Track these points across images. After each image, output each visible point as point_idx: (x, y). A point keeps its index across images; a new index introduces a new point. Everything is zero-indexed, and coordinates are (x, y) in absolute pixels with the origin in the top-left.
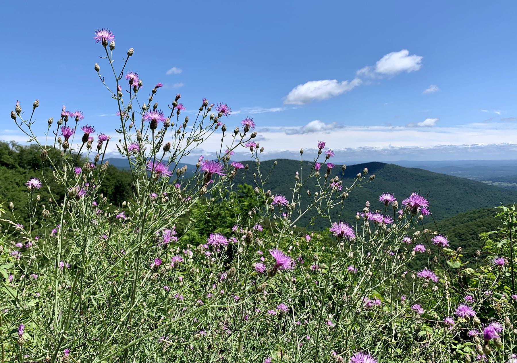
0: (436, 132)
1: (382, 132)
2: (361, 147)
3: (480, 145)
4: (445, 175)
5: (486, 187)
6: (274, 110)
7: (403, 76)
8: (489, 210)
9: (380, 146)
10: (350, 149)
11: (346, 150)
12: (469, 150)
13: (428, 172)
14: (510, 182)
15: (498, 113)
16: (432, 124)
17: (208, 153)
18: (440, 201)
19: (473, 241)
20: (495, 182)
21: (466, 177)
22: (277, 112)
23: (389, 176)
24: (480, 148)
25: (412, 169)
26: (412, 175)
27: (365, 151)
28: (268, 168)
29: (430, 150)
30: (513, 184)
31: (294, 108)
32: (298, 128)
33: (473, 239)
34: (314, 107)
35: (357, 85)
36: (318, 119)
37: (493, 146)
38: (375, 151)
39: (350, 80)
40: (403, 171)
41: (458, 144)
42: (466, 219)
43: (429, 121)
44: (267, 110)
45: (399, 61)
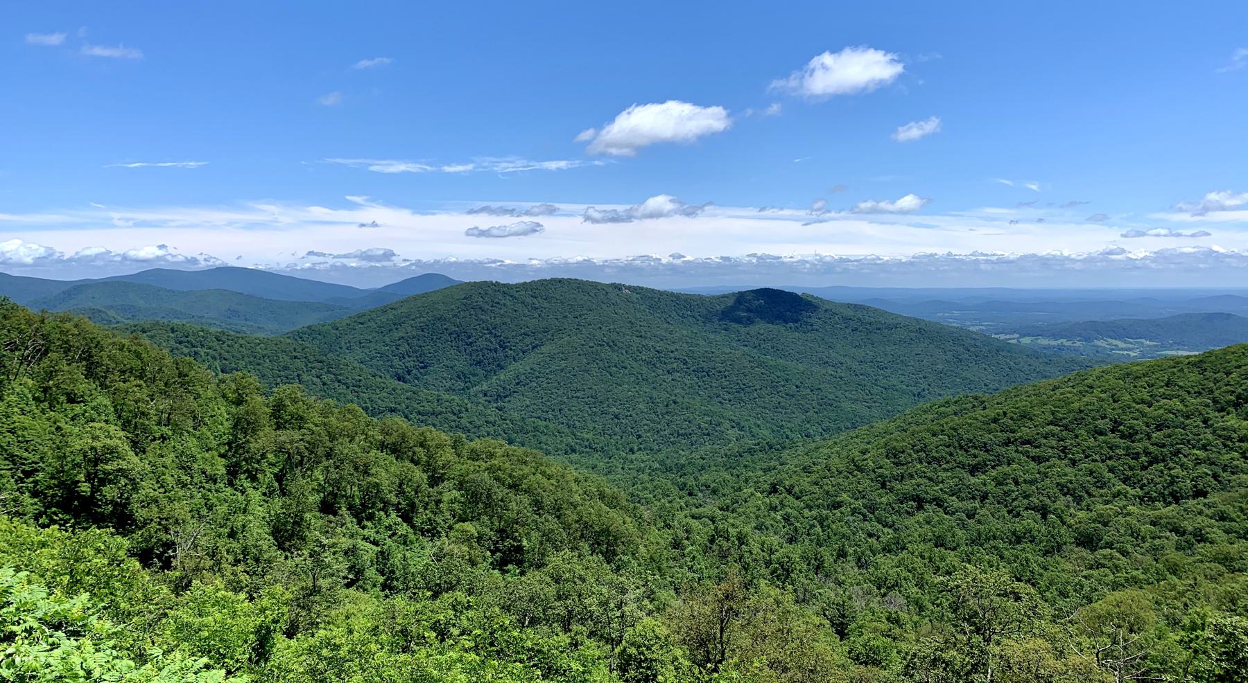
0: (909, 225)
2: (754, 255)
4: (917, 321)
5: (1004, 348)
6: (553, 165)
8: (976, 398)
10: (727, 259)
12: (983, 266)
13: (884, 313)
14: (1055, 336)
15: (1034, 187)
19: (919, 466)
20: (1025, 336)
22: (559, 169)
25: (849, 306)
26: (847, 319)
27: (766, 263)
28: (529, 300)
30: (1059, 342)
32: (621, 208)
33: (921, 462)
34: (660, 163)
36: (667, 193)
41: (961, 251)
43: (908, 201)
44: (537, 166)
45: (857, 69)
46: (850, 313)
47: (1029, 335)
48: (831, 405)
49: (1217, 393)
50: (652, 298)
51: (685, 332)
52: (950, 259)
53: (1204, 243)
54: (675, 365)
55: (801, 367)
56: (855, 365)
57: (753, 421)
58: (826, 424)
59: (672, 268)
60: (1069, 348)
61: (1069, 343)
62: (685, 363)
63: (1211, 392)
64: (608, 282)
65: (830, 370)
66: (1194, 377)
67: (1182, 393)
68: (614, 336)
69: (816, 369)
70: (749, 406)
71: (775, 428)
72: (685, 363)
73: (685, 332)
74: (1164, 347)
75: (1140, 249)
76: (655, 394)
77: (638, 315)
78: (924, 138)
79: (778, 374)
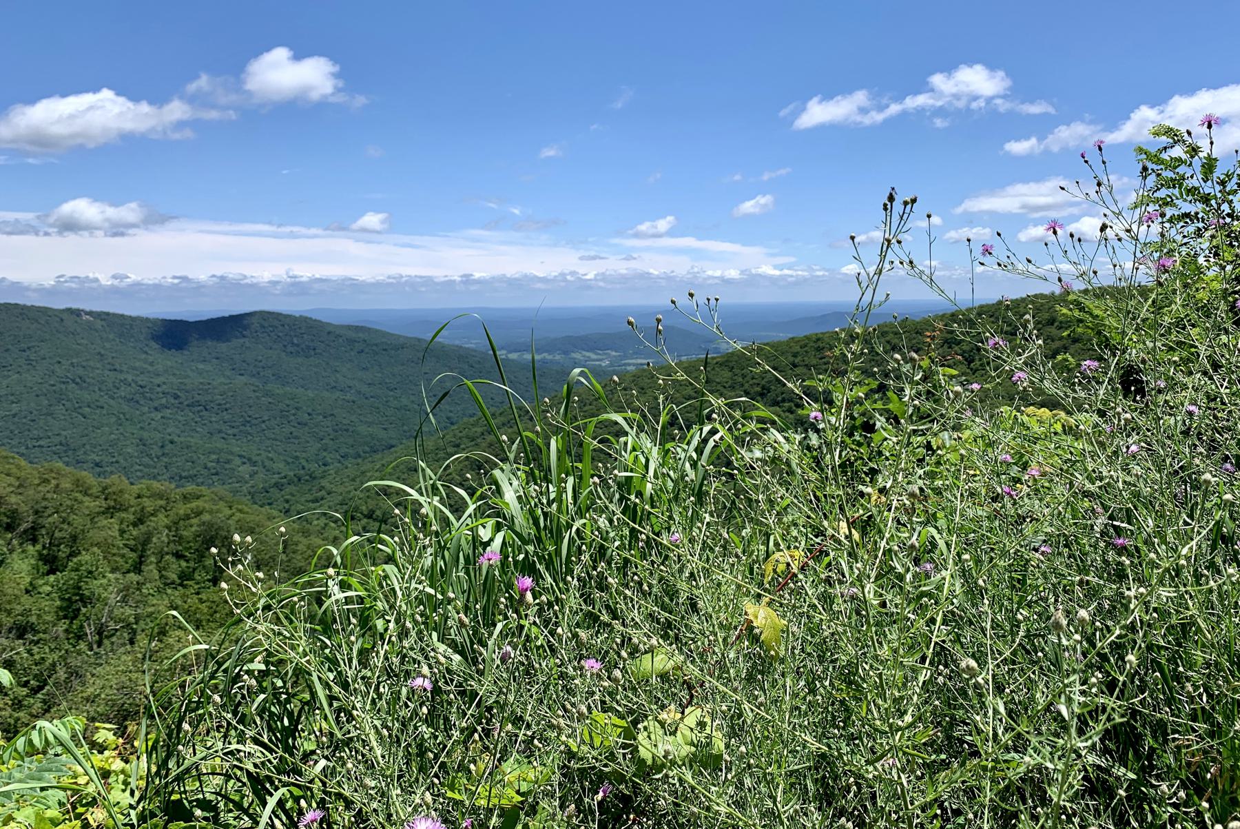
0: (395, 245)
1: (263, 239)
2: (214, 276)
3: (477, 275)
7: (294, 112)
9: (264, 273)
10: (184, 279)
11: (176, 281)
15: (516, 212)
16: (378, 227)
17: (175, 277)
18: (412, 398)
20: (510, 352)
21: (457, 342)
23: (298, 345)
24: (479, 282)
25: (349, 327)
26: (351, 341)
29: (378, 285)
31: (31, 161)
35: (1063, 128)
37: (502, 279)
38: (253, 286)
39: (159, 100)
40: (329, 333)
41: (439, 273)
42: (479, 430)
43: (372, 220)
45: (283, 73)
46: (352, 335)
47: (516, 351)
48: (347, 430)
49: (747, 386)
50: (122, 325)
51: (169, 363)
52: (428, 281)
53: (633, 265)
54: (164, 401)
55: (311, 394)
56: (365, 389)
57: (264, 454)
58: (343, 451)
59: (113, 291)
60: (551, 361)
61: (550, 357)
62: (176, 397)
63: (742, 385)
64: (62, 307)
65: (338, 394)
66: (727, 374)
67: (719, 387)
68: (80, 371)
69: (326, 394)
70: (257, 439)
71: (290, 460)
72: (176, 397)
73: (169, 363)
74: (625, 357)
75: (590, 271)
76: (145, 435)
77: (108, 345)
78: (887, 122)
79: (287, 402)
